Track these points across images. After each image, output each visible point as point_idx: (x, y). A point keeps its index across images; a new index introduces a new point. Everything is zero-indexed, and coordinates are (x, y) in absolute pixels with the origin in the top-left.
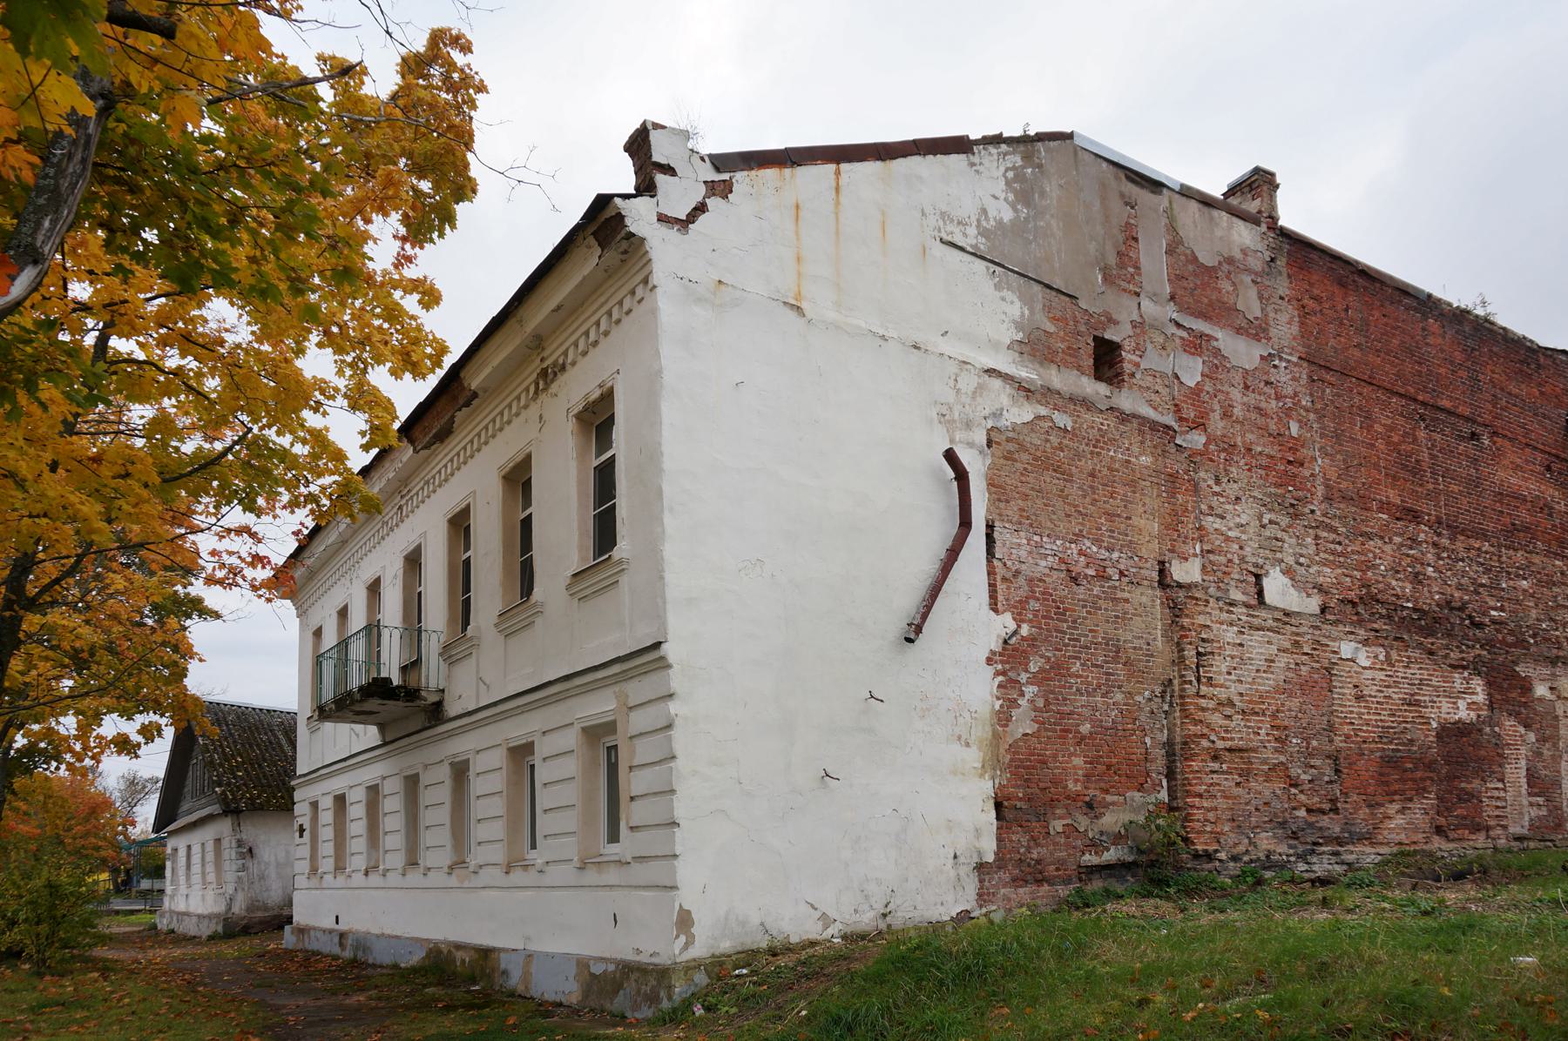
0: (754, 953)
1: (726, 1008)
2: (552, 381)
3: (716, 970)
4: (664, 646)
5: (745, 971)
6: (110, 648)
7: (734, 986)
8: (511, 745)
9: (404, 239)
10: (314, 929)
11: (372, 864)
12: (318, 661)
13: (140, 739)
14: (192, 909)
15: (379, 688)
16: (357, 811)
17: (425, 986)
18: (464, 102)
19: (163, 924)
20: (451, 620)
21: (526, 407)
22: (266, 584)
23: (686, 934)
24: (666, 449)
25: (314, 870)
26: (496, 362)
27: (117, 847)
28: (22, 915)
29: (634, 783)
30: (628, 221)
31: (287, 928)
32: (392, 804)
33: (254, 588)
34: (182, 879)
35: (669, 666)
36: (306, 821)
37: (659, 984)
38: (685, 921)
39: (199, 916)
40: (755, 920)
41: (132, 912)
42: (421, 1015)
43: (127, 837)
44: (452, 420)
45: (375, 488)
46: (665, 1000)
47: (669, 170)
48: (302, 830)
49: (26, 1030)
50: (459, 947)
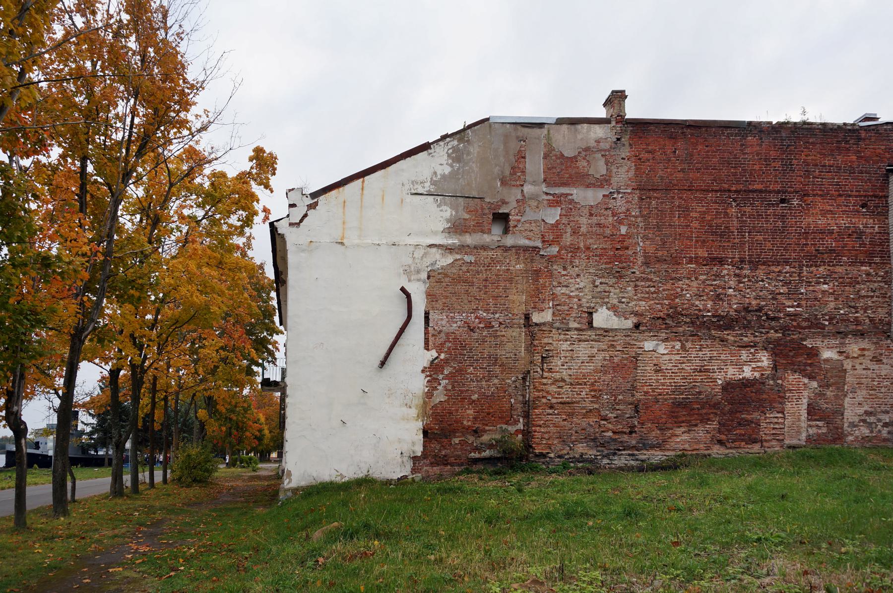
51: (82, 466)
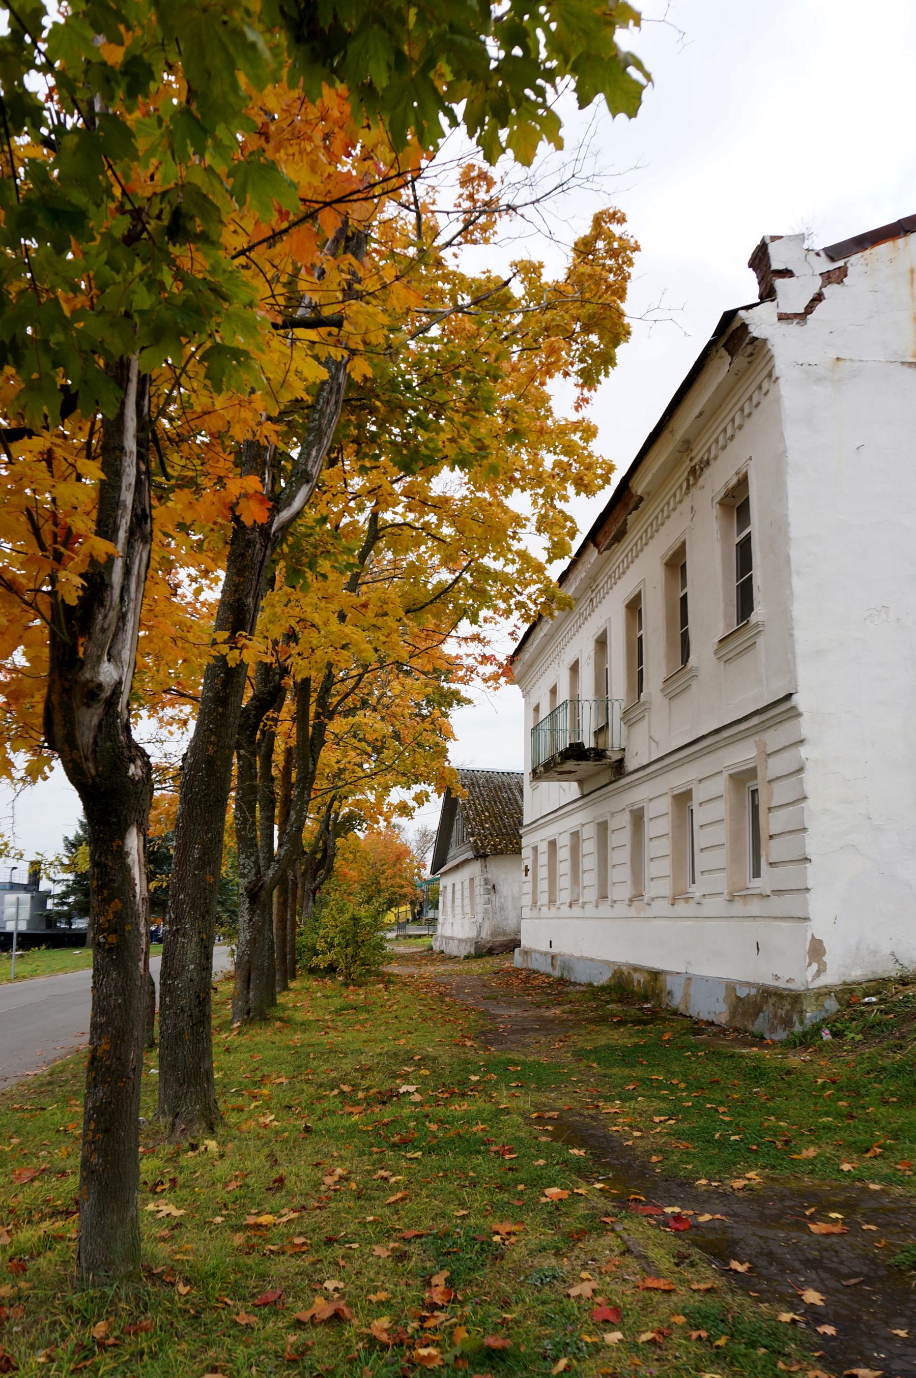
0: (885, 981)
1: (852, 1035)
2: (700, 476)
3: (847, 996)
4: (794, 697)
5: (874, 999)
6: (397, 736)
7: (862, 1013)
8: (675, 793)
9: (582, 386)
10: (535, 951)
11: (575, 898)
12: (535, 730)
13: (415, 804)
14: (455, 935)
15: (576, 752)
16: (564, 854)
17: (608, 1003)
18: (624, 263)
19: (437, 946)
20: (629, 690)
21: (681, 502)
22: (495, 677)
23: (817, 962)
24: (791, 519)
25: (535, 902)
26: (654, 470)
27: (414, 886)
28: (336, 942)
29: (773, 823)
30: (751, 328)
31: (517, 950)
32: (589, 847)
33: (485, 681)
34: (449, 910)
35: (800, 715)
36: (528, 862)
37: (793, 1008)
38: (817, 950)
39: (460, 941)
40: (886, 949)
41: (420, 936)
42: (598, 1028)
43: (420, 877)
44: (625, 523)
45: (570, 590)
46: (797, 1024)
47: (786, 273)
48: (527, 870)
49: (328, 1027)
50: (636, 969)
51: (48, 948)
